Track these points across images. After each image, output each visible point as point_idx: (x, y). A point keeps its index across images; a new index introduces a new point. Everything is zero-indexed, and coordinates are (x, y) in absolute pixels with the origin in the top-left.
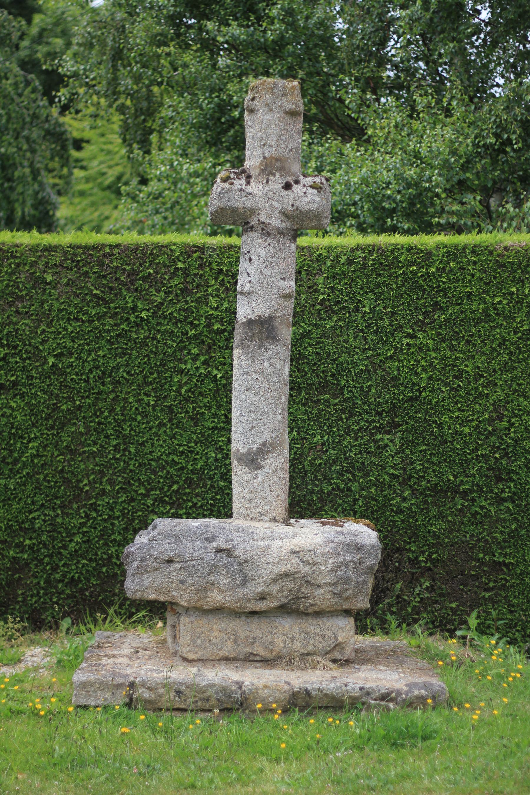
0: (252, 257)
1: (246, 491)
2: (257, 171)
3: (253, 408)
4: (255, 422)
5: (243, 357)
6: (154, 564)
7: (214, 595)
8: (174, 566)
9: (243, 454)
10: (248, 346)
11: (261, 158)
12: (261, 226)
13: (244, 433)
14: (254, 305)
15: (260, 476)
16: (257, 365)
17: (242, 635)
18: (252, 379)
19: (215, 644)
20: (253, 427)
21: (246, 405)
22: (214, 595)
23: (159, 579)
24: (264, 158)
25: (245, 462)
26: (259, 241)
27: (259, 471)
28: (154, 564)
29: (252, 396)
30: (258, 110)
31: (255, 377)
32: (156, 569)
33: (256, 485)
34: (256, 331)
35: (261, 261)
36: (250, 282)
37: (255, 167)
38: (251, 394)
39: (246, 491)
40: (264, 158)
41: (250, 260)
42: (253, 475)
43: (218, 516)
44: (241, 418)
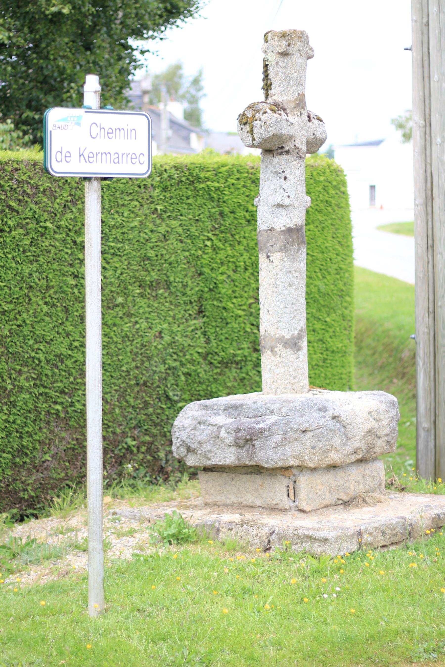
0: (287, 176)
1: (291, 370)
2: (293, 105)
3: (294, 301)
4: (296, 313)
5: (285, 259)
6: (295, 436)
7: (331, 455)
8: (309, 435)
9: (288, 340)
10: (290, 250)
11: (297, 95)
12: (297, 150)
13: (288, 322)
14: (292, 215)
15: (300, 356)
16: (296, 265)
17: (333, 484)
18: (293, 277)
19: (320, 496)
20: (295, 317)
21: (289, 298)
22: (331, 455)
23: (298, 446)
24: (299, 94)
25: (290, 346)
26: (295, 163)
27: (300, 352)
28: (295, 436)
29: (293, 291)
30: (293, 55)
31: (295, 275)
32: (296, 440)
33: (298, 364)
34: (295, 237)
35: (296, 179)
36: (289, 197)
37: (290, 102)
38: (292, 290)
39: (291, 370)
40: (299, 94)
41: (285, 178)
42: (296, 356)
43: (342, 388)
44: (285, 310)
